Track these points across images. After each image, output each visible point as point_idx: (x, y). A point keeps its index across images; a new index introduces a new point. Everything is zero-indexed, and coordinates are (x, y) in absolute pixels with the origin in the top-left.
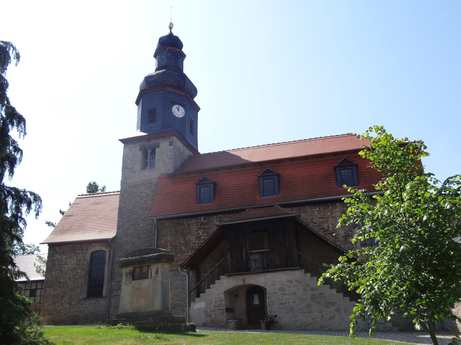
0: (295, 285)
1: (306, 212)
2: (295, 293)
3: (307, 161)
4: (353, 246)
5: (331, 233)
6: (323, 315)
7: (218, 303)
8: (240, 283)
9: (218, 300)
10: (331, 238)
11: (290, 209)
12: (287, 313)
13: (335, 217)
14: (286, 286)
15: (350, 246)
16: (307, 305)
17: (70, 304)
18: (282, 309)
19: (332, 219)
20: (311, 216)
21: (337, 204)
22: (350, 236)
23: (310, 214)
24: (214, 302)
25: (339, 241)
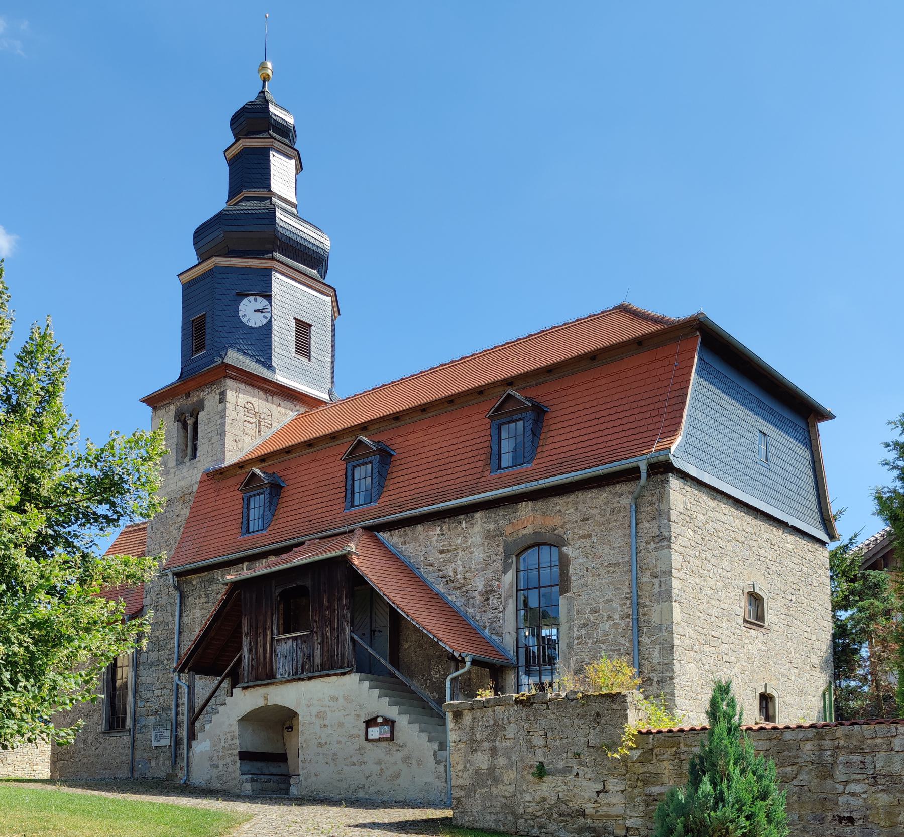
1: (415, 539)
2: (341, 724)
3: (426, 416)
5: (460, 586)
6: (382, 770)
7: (229, 742)
8: (261, 703)
9: (229, 735)
11: (389, 533)
13: (470, 547)
14: (327, 709)
15: (492, 615)
16: (359, 749)
18: (323, 754)
19: (463, 553)
20: (424, 549)
21: (478, 515)
23: (424, 544)
24: (223, 740)
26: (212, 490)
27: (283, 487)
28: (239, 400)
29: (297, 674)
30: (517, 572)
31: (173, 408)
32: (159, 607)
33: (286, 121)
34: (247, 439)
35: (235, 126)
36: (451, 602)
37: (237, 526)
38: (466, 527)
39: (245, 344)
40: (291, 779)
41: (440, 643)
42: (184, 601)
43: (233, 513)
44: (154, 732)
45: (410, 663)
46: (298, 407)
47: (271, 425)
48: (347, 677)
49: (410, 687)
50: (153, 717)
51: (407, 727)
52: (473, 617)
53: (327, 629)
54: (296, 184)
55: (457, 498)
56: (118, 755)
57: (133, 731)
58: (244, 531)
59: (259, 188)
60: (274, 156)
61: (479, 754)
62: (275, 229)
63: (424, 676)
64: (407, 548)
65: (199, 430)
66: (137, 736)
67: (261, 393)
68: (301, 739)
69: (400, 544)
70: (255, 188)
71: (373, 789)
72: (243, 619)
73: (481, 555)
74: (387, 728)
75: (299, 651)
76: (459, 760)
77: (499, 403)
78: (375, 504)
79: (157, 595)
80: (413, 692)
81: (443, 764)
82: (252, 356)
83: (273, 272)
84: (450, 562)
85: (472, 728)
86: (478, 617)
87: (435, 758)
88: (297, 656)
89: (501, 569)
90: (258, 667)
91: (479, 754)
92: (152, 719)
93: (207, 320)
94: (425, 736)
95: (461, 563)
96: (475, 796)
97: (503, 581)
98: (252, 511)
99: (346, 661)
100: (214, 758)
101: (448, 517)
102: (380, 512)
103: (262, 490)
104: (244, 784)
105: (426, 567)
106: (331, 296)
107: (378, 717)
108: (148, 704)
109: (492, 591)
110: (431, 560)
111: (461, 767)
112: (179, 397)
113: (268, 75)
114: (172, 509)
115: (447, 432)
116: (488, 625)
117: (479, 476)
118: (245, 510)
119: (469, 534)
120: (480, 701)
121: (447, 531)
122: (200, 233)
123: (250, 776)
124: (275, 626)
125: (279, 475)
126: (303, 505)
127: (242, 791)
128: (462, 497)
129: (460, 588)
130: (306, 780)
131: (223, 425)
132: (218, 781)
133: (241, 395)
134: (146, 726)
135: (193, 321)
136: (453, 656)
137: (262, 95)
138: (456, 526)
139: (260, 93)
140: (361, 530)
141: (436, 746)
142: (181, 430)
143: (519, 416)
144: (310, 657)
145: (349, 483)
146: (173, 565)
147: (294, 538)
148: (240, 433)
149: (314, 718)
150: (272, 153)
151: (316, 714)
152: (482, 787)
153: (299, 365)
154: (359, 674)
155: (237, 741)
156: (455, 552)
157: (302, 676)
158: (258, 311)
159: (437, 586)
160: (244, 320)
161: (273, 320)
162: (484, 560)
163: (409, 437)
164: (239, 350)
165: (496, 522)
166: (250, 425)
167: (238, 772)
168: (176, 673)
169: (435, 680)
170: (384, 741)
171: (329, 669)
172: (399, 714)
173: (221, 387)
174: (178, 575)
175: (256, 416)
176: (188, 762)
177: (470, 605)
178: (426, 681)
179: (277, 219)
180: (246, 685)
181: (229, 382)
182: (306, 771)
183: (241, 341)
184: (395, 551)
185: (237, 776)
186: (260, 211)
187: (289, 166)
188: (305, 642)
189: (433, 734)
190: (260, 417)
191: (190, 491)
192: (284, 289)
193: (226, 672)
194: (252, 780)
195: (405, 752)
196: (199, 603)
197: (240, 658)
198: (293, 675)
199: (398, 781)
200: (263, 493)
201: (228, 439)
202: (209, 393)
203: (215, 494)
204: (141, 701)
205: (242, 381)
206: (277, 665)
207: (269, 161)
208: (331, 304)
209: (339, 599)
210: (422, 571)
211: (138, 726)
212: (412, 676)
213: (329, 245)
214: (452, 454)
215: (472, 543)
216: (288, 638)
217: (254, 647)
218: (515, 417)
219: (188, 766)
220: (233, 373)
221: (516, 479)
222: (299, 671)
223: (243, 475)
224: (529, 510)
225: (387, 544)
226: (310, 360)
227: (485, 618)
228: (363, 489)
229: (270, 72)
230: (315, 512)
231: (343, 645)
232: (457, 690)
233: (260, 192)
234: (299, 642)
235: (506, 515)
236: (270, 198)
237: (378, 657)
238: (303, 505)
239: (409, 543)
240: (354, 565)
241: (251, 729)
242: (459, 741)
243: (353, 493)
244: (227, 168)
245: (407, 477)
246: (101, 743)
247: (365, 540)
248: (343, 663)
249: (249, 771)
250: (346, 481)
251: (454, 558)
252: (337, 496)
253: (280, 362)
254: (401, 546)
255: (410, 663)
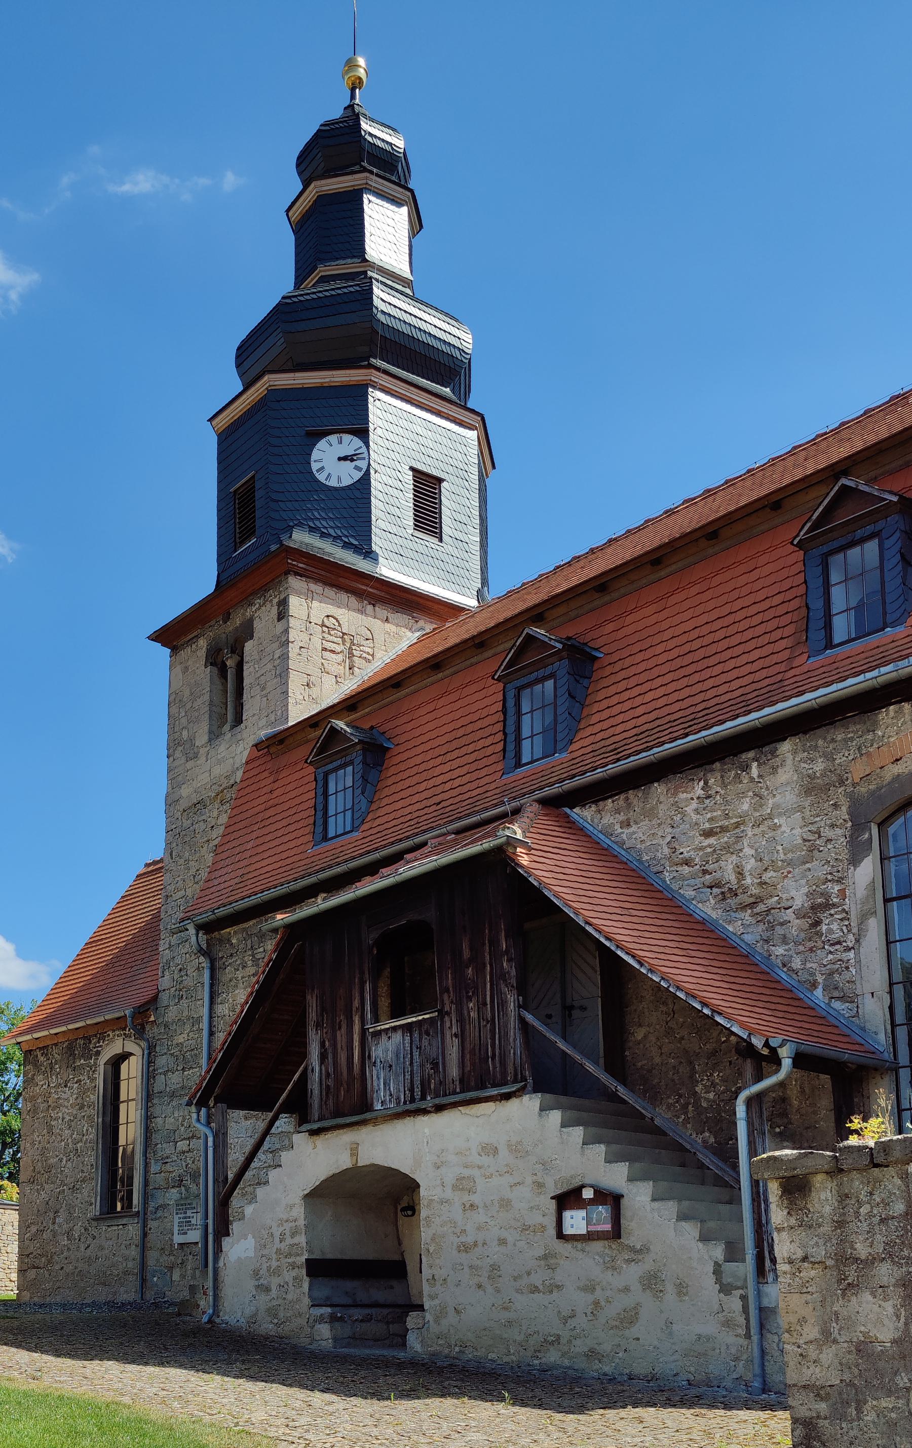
0: (507, 1165)
1: (650, 814)
4: (845, 956)
5: (752, 900)
6: (596, 1303)
7: (289, 1241)
8: (345, 1162)
9: (288, 1226)
10: (750, 930)
11: (594, 808)
12: (480, 1286)
13: (770, 817)
14: (476, 1172)
15: (831, 957)
16: (545, 1257)
17: (69, 1234)
18: (471, 1267)
20: (670, 830)
21: (786, 747)
22: (834, 905)
23: (669, 821)
25: (784, 940)
26: (266, 774)
27: (388, 749)
28: (313, 613)
29: (413, 1100)
30: (882, 860)
31: (203, 643)
32: (183, 993)
33: (391, 144)
34: (329, 681)
35: (303, 167)
36: (733, 938)
37: (308, 830)
38: (760, 776)
39: (324, 519)
40: (408, 1319)
41: (719, 1019)
42: (218, 974)
43: (301, 807)
44: (176, 1218)
45: (650, 1071)
46: (421, 623)
47: (373, 655)
48: (514, 1103)
49: (652, 1119)
50: (174, 1191)
51: (648, 1208)
52: (784, 965)
53: (471, 1005)
54: (410, 255)
55: (737, 717)
56: (121, 1260)
57: (143, 1217)
58: (319, 837)
59: (344, 258)
60: (370, 201)
61: (867, 1296)
62: (373, 317)
63: (680, 1096)
64: (634, 833)
65: (245, 674)
66: (152, 1224)
67: (353, 600)
68: (426, 1234)
69: (617, 827)
70: (337, 259)
71: (580, 1346)
72: (309, 997)
73: (797, 831)
74: (603, 1211)
75: (416, 1054)
76: (807, 1312)
77: (821, 509)
78: (564, 755)
79: (181, 970)
80: (659, 1132)
81: (738, 1293)
82: (336, 538)
83: (370, 390)
84: (728, 852)
85: (840, 1224)
86: (797, 963)
87: (718, 1280)
88: (411, 1064)
89: (844, 855)
90: (338, 1090)
91: (867, 1296)
92: (174, 1194)
93: (258, 485)
94: (691, 1230)
95: (753, 852)
96: (859, 1419)
97: (851, 881)
98: (332, 799)
99: (510, 1069)
100: (261, 1272)
101: (719, 760)
102: (574, 767)
103: (348, 758)
104: (318, 1326)
105: (675, 868)
106: (476, 429)
107: (583, 1186)
108: (168, 1167)
109: (827, 906)
110: (686, 851)
111: (811, 1332)
112: (212, 623)
113: (360, 78)
114: (203, 817)
115: (709, 595)
116: (820, 979)
117: (782, 667)
118: (320, 799)
119: (767, 788)
120: (860, 1149)
121: (719, 789)
122: (244, 348)
123: (329, 1310)
124: (368, 1007)
125: (381, 730)
126: (425, 775)
127: (313, 1340)
128: (750, 712)
129: (752, 905)
130: (437, 1320)
131: (285, 657)
132: (269, 1319)
133: (315, 604)
134: (164, 1206)
135: (235, 491)
136: (750, 1045)
137: (349, 110)
138: (737, 776)
139: (345, 108)
140: (536, 806)
141: (718, 1252)
142: (217, 681)
143: (870, 529)
144: (437, 1063)
145: (511, 721)
146: (196, 911)
147: (408, 837)
148: (315, 672)
149: (449, 1190)
150: (366, 197)
151: (454, 1182)
152: (879, 1394)
153: (421, 549)
154: (539, 1095)
155: (302, 1239)
156: (737, 831)
157: (423, 1105)
158: (345, 458)
159: (700, 905)
160: (321, 477)
161: (372, 472)
162: (805, 840)
163: (630, 619)
164: (312, 530)
165: (829, 757)
166: (334, 656)
167: (306, 1301)
168: (193, 1106)
169: (704, 1104)
170: (598, 1239)
171: (477, 1089)
172: (631, 1179)
173: (280, 592)
174: (206, 928)
175: (344, 641)
176: (215, 1279)
177: (777, 940)
178: (685, 1107)
179: (374, 297)
180: (315, 1126)
181: (294, 582)
182: (436, 1302)
183: (316, 514)
184: (607, 841)
185: (305, 1309)
186: (345, 290)
187: (397, 217)
188: (428, 1034)
189: (711, 1224)
190: (352, 643)
191: (232, 782)
192: (390, 418)
193: (280, 1101)
194: (333, 1319)
195: (647, 1265)
196: (243, 978)
197: (304, 1074)
198: (405, 1103)
199: (634, 1331)
200: (351, 763)
201: (293, 681)
202: (260, 606)
203: (271, 779)
204: (157, 1161)
205: (317, 580)
206: (375, 1084)
207: (362, 211)
208: (476, 443)
209: (494, 943)
210: (667, 876)
211: (152, 1205)
212: (653, 1096)
213: (471, 341)
214: (721, 634)
215: (776, 806)
216: (394, 1029)
217: (330, 1051)
218: (859, 534)
219: (216, 1287)
220: (301, 565)
221: (871, 659)
222: (418, 1093)
223: (320, 733)
224: (904, 723)
225: (591, 829)
226: (441, 540)
227: (814, 966)
228: (538, 728)
229: (362, 73)
230: (448, 786)
231: (504, 1036)
232: (762, 1124)
233: (348, 266)
234: (416, 1035)
235: (852, 739)
236: (365, 273)
237: (578, 1057)
238: (425, 775)
239: (636, 823)
240: (522, 866)
241: (330, 1213)
242: (805, 1259)
243: (518, 740)
244: (291, 238)
245: (627, 695)
246: (94, 1238)
247: (547, 823)
248: (504, 1073)
249: (328, 1298)
250: (505, 721)
251: (736, 842)
252: (489, 751)
253: (386, 545)
254: (620, 830)
255: (650, 1071)
